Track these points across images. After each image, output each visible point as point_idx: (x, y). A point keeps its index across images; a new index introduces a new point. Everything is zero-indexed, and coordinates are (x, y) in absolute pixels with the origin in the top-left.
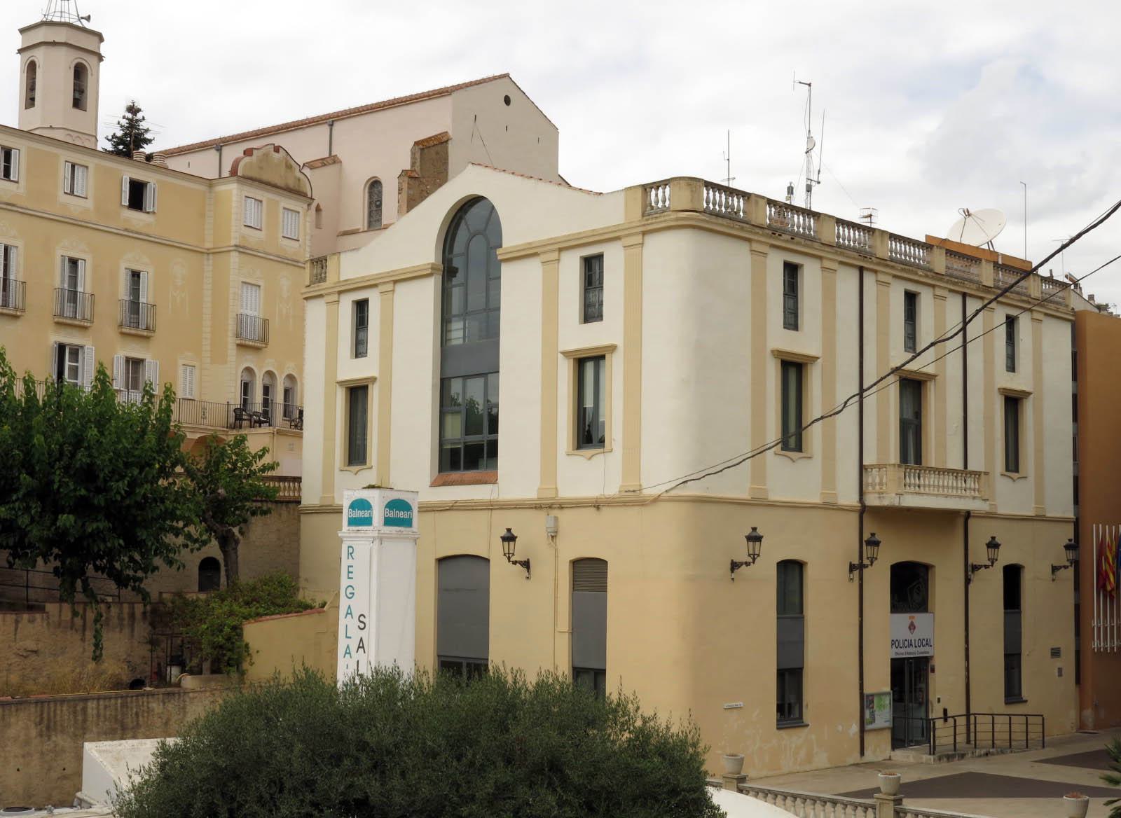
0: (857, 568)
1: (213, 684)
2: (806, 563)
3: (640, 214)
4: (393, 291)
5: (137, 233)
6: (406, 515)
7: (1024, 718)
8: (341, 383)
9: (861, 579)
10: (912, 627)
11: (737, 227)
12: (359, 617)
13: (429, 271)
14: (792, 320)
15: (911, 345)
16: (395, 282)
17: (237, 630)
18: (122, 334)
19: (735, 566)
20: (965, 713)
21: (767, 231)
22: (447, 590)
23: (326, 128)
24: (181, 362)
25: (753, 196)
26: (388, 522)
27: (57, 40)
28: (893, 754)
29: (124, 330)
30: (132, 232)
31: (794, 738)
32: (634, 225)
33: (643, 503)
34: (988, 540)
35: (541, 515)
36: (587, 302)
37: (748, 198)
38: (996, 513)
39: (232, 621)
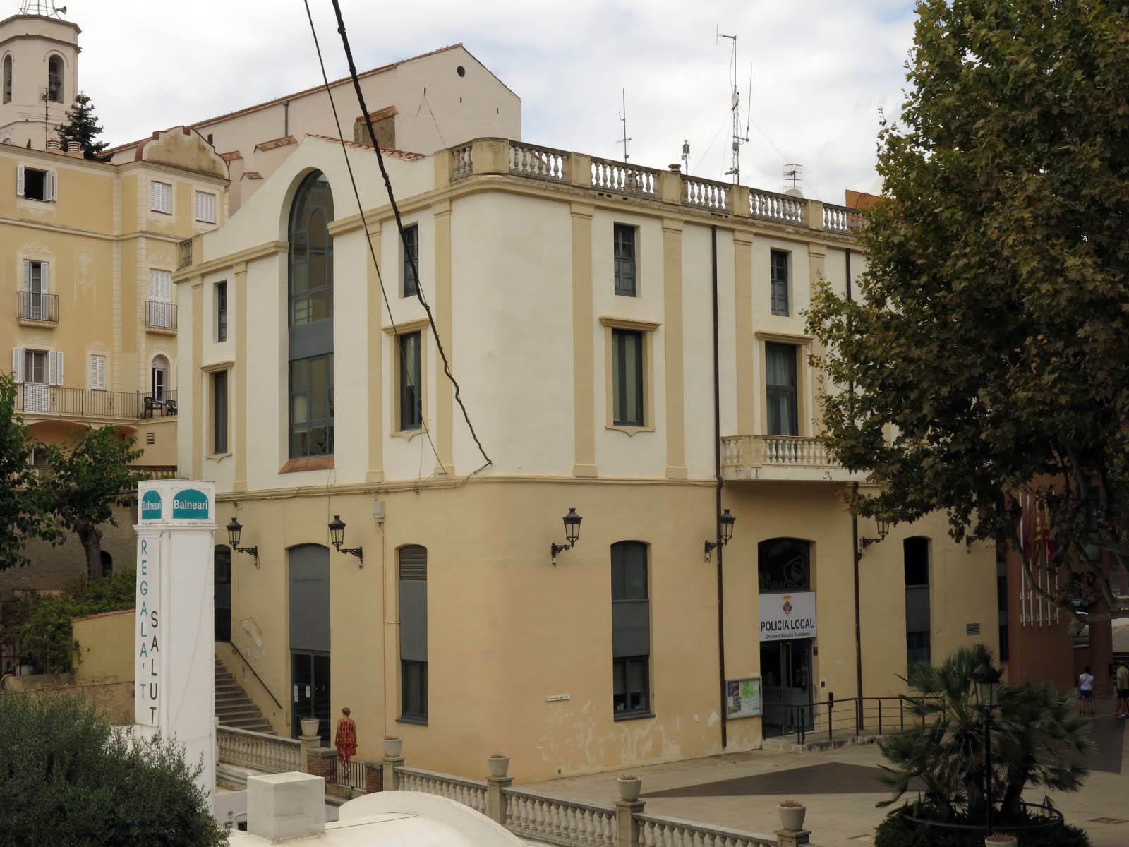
0: (715, 547)
1: (38, 685)
2: (650, 544)
4: (246, 271)
5: (35, 223)
6: (200, 506)
7: (877, 701)
8: (204, 369)
9: (720, 559)
10: (787, 607)
11: (552, 189)
13: (273, 250)
14: (627, 284)
15: (783, 307)
16: (247, 262)
18: (22, 326)
19: (555, 550)
20: (857, 696)
21: (592, 192)
23: (281, 109)
24: (89, 352)
25: (572, 154)
27: (30, 34)
28: (764, 742)
29: (23, 322)
30: (29, 222)
31: (637, 730)
32: (441, 191)
37: (568, 157)
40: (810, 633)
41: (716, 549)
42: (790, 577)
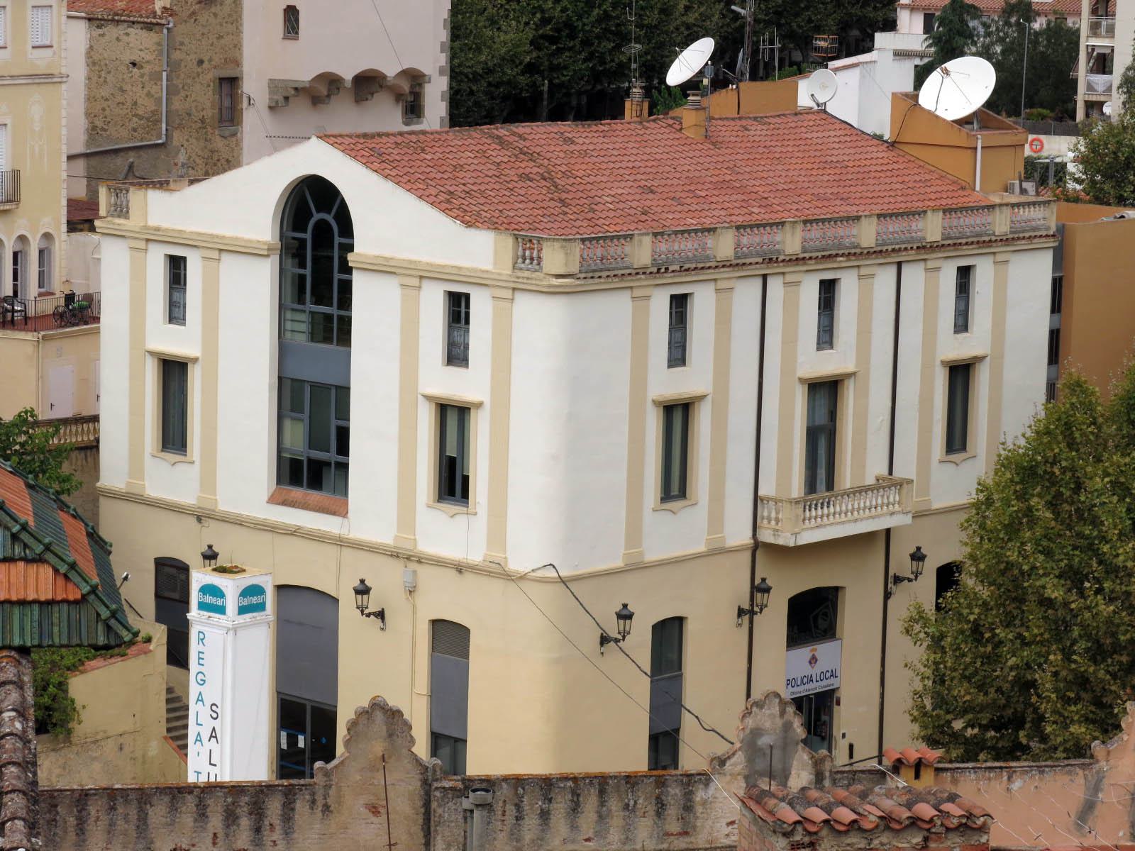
0: (748, 613)
3: (511, 265)
9: (751, 622)
12: (198, 673)
15: (827, 339)
17: (62, 686)
22: (288, 621)
26: (242, 610)
33: (508, 577)
34: (913, 550)
35: (397, 565)
36: (451, 341)
38: (930, 510)
39: (55, 678)
40: (834, 683)
41: (747, 616)
42: (816, 627)
